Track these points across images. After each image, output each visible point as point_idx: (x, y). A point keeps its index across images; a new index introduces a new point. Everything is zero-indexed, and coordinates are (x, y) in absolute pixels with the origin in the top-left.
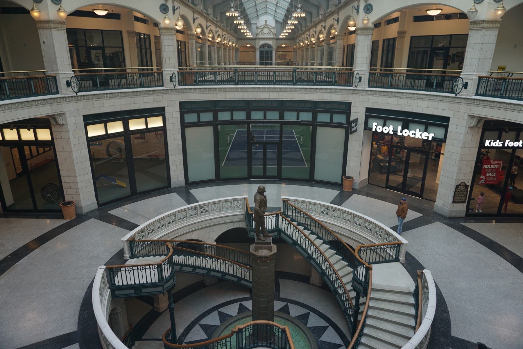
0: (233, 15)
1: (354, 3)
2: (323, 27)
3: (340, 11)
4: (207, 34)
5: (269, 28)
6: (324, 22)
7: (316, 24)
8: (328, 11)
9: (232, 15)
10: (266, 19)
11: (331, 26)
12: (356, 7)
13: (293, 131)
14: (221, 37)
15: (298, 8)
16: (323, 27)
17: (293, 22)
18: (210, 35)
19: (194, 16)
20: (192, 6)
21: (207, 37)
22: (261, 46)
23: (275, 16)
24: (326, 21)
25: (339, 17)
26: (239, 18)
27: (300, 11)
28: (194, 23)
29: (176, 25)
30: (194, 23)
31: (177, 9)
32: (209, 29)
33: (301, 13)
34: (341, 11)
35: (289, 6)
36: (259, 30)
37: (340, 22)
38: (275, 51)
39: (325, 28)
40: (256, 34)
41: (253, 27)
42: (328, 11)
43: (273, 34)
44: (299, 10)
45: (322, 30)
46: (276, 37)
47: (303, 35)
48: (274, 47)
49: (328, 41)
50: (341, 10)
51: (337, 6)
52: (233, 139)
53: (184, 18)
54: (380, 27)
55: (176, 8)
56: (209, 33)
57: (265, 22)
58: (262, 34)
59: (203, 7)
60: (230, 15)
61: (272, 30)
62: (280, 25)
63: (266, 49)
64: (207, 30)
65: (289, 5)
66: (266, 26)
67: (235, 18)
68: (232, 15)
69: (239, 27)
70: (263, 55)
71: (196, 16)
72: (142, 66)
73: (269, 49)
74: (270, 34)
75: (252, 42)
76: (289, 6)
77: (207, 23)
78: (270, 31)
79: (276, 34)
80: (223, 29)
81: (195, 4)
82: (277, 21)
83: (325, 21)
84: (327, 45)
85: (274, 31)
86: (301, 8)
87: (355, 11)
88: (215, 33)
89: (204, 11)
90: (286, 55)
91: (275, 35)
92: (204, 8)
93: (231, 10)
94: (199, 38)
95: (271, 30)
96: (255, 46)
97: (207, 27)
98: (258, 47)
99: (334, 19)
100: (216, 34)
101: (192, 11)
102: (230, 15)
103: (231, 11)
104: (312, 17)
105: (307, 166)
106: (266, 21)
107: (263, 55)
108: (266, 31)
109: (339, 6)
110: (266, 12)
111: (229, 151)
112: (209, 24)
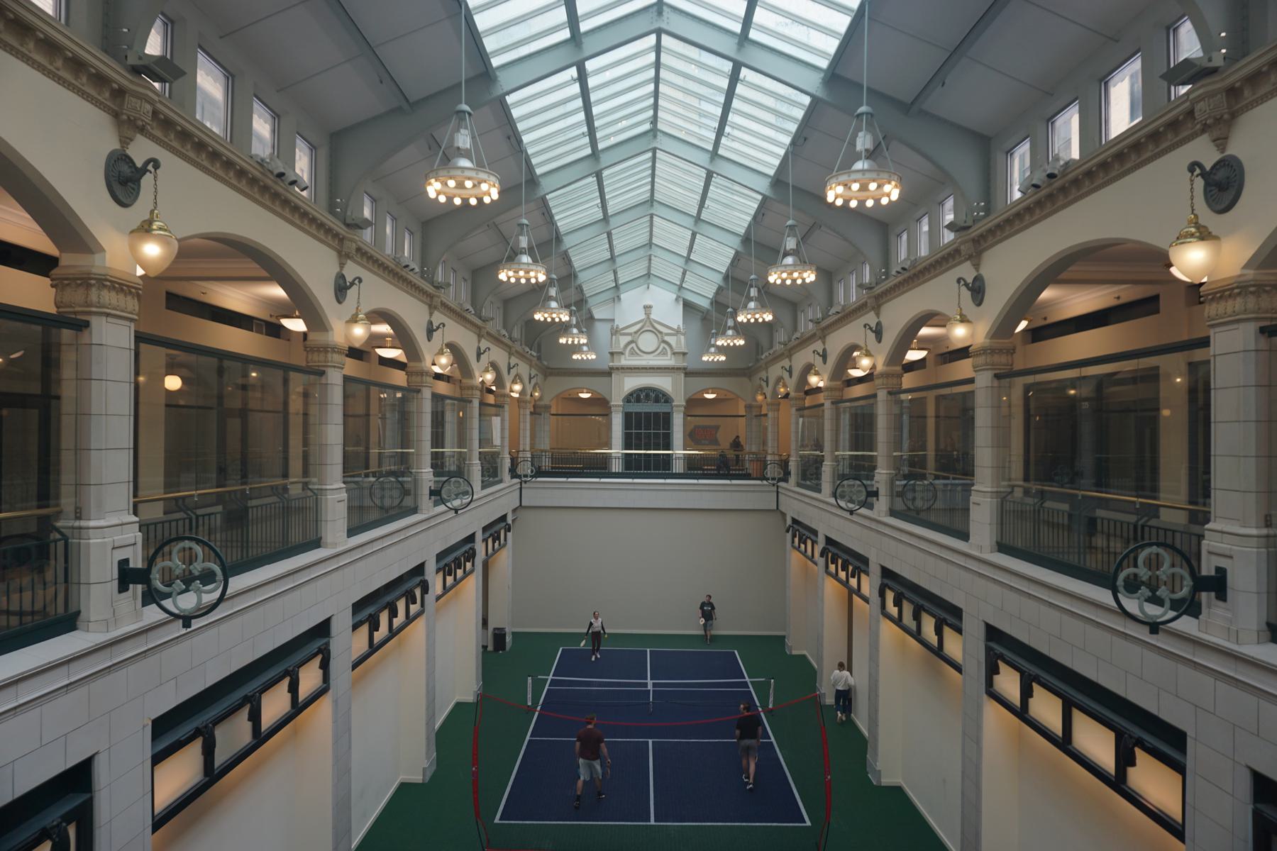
0: (576, 342)
1: (783, 361)
3: (829, 334)
4: (508, 385)
5: (661, 333)
6: (872, 313)
7: (824, 329)
8: (798, 335)
9: (573, 342)
10: (648, 303)
11: (808, 369)
12: (873, 326)
13: (736, 652)
14: (522, 382)
15: (751, 299)
17: (717, 357)
19: (480, 345)
20: (510, 343)
21: (508, 390)
22: (631, 394)
23: (681, 287)
25: (827, 346)
27: (733, 332)
28: (478, 361)
29: (434, 364)
30: (478, 361)
32: (513, 372)
33: (733, 337)
34: (832, 335)
36: (624, 340)
38: (681, 415)
39: (824, 356)
40: (612, 354)
41: (602, 330)
42: (798, 335)
43: (674, 354)
44: (752, 305)
45: (784, 376)
47: (787, 360)
48: (679, 400)
49: (837, 394)
51: (871, 288)
52: (528, 738)
53: (454, 349)
55: (435, 328)
56: (514, 382)
58: (633, 353)
59: (501, 325)
60: (567, 341)
62: (696, 325)
65: (712, 303)
66: (648, 325)
67: (564, 328)
68: (573, 342)
69: (503, 276)
72: (461, 452)
73: (660, 408)
74: (664, 353)
75: (598, 383)
76: (721, 284)
78: (665, 342)
79: (684, 354)
80: (431, 296)
81: (483, 318)
82: (688, 306)
83: (825, 337)
84: (832, 403)
85: (678, 341)
87: (872, 336)
88: (526, 380)
89: (504, 332)
90: (717, 428)
92: (505, 327)
93: (549, 305)
94: (490, 391)
95: (666, 338)
96: (608, 397)
97: (509, 369)
98: (617, 400)
99: (814, 352)
100: (530, 382)
101: (475, 333)
102: (567, 341)
105: (808, 823)
106: (647, 308)
108: (648, 342)
110: (648, 275)
111: (548, 690)
112: (514, 360)
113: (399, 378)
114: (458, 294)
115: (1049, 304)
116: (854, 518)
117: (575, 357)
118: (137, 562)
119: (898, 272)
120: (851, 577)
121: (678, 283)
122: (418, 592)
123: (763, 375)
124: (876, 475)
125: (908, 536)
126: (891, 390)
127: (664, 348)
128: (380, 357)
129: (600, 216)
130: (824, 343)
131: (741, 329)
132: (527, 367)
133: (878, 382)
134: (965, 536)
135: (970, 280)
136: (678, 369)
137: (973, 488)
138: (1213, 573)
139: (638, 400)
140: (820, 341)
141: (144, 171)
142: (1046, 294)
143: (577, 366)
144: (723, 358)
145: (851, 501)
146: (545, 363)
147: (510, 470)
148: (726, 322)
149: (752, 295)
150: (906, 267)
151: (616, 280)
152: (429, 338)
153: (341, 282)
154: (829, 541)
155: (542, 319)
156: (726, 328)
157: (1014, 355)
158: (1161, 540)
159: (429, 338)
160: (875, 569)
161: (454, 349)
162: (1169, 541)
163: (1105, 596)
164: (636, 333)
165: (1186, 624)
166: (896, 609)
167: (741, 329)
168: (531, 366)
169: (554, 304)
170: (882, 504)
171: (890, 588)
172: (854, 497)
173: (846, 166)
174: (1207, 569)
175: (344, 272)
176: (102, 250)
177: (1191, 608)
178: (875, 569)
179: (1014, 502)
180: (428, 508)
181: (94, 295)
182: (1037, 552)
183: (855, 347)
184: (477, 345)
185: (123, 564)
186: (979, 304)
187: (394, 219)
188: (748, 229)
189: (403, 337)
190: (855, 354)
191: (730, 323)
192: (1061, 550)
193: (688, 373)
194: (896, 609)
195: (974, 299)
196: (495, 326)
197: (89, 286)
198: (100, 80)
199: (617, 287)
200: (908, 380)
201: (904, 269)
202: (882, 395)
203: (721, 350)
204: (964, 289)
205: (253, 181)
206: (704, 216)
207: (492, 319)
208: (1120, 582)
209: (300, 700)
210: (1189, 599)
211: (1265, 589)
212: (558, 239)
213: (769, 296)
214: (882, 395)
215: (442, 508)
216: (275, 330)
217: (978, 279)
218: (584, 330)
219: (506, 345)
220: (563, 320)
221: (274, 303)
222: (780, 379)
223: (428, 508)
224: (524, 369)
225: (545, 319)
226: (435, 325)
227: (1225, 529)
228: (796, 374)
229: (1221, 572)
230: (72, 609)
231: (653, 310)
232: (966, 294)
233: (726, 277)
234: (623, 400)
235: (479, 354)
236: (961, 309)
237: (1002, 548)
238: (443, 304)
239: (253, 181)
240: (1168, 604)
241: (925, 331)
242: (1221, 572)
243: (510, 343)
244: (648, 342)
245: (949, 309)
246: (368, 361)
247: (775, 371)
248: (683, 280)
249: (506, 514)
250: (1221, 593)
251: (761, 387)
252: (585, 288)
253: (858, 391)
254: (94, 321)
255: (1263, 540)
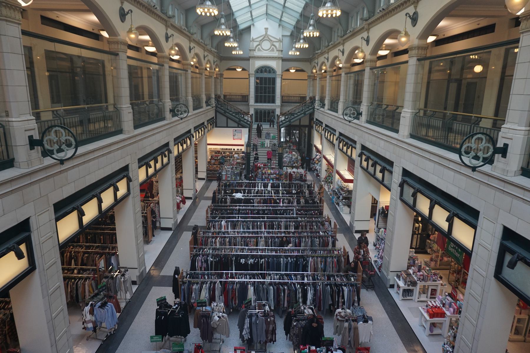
2: (341, 51)
4: (204, 65)
5: (271, 41)
11: (323, 63)
12: (366, 38)
14: (210, 63)
15: (310, 25)
16: (341, 51)
18: (208, 66)
19: (191, 45)
20: (204, 45)
24: (330, 53)
25: (369, 35)
26: (232, 40)
31: (171, 36)
32: (206, 59)
35: (293, 30)
36: (255, 44)
37: (346, 54)
39: (343, 53)
40: (250, 50)
43: (277, 51)
44: (311, 28)
46: (282, 56)
47: (342, 46)
48: (279, 71)
49: (331, 73)
50: (347, 42)
54: (494, 32)
56: (207, 64)
57: (264, 31)
58: (259, 50)
59: (200, 37)
61: (277, 44)
63: (265, 75)
64: (204, 60)
69: (233, 53)
70: (269, 97)
71: (192, 45)
74: (273, 50)
75: (243, 64)
76: (293, 30)
77: (190, 44)
79: (282, 51)
83: (369, 29)
86: (313, 26)
87: (365, 43)
88: (212, 63)
89: (201, 41)
91: (280, 52)
93: (206, 3)
95: (274, 43)
97: (204, 57)
98: (406, 287)
99: (406, 15)
103: (230, 41)
104: (322, 42)
106: (266, 29)
107: (269, 97)
109: (370, 21)
113: (155, 60)
114: (179, 21)
115: (443, 29)
116: (351, 124)
117: (233, 53)
118: (36, 137)
119: (380, 11)
120: (508, 266)
121: (280, 18)
122: (166, 153)
123: (316, 61)
124: (402, 112)
125: (386, 137)
126: (419, 57)
127: (273, 48)
128: (146, 51)
129: (248, 4)
130: (343, 46)
131: (297, 49)
132: (213, 57)
133: (328, 73)
134: (397, 131)
135: (411, 14)
136: (279, 58)
137: (502, 126)
138: (502, 146)
139: (261, 72)
140: (366, 32)
141: (128, 13)
142: (442, 24)
143: (234, 56)
144: (298, 53)
145: (476, 158)
146: (221, 55)
147: (206, 102)
148: (300, 36)
149: (311, 23)
150: (385, 8)
151: (252, 16)
152: (190, 52)
153: (122, 11)
154: (341, 134)
155: (218, 34)
156: (300, 39)
157: (428, 50)
158: (482, 131)
159: (190, 52)
160: (358, 146)
161: (197, 55)
162: (488, 133)
163: (455, 157)
164: (261, 40)
165: (487, 168)
166: (381, 174)
167: (306, 39)
168: (214, 57)
169: (223, 27)
170: (364, 118)
171: (371, 159)
172: (480, 154)
173: (299, 41)
174: (500, 144)
175: (123, 7)
176: (119, 35)
177: (490, 161)
178: (358, 146)
179: (419, 116)
180: (192, 112)
181: (165, 59)
182: (446, 144)
183: (357, 48)
184: (165, 31)
185: (30, 138)
186: (414, 26)
187: (177, 10)
188: (302, 12)
189: (155, 42)
190: (356, 52)
191: (302, 37)
192: (439, 138)
193: (284, 60)
194: (381, 174)
195: (412, 23)
196: (197, 37)
197: (118, 44)
198: (163, 19)
199: (252, 20)
200: (379, 63)
201: (383, 9)
202: (367, 70)
203: (297, 49)
204: (408, 18)
205: (146, 8)
206: (286, 5)
207: (195, 33)
208: (463, 150)
209: (118, 198)
210: (490, 158)
211: (527, 153)
212: (233, 14)
213: (320, 23)
214: (367, 70)
215: (176, 118)
216: (97, 37)
217: (416, 13)
218: (238, 40)
219: (203, 46)
220: (228, 35)
221: (93, 23)
222: (323, 63)
223: (192, 112)
224: (211, 57)
225: (220, 34)
226: (169, 35)
227: (511, 127)
228: (330, 60)
229: (506, 146)
230: (11, 157)
231: (268, 31)
232: (409, 21)
233: (301, 15)
234: (255, 72)
235: (190, 50)
236: (406, 28)
237: (412, 136)
238: (172, 25)
239: (146, 8)
240: (481, 159)
241: (388, 41)
242: (506, 146)
243: (204, 45)
244: (266, 45)
245: (401, 29)
246: (141, 52)
247: (321, 59)
248: (282, 17)
249: (29, 218)
250: (504, 155)
251: (315, 66)
252: (238, 20)
253: (357, 68)
254: (120, 54)
255: (527, 132)
